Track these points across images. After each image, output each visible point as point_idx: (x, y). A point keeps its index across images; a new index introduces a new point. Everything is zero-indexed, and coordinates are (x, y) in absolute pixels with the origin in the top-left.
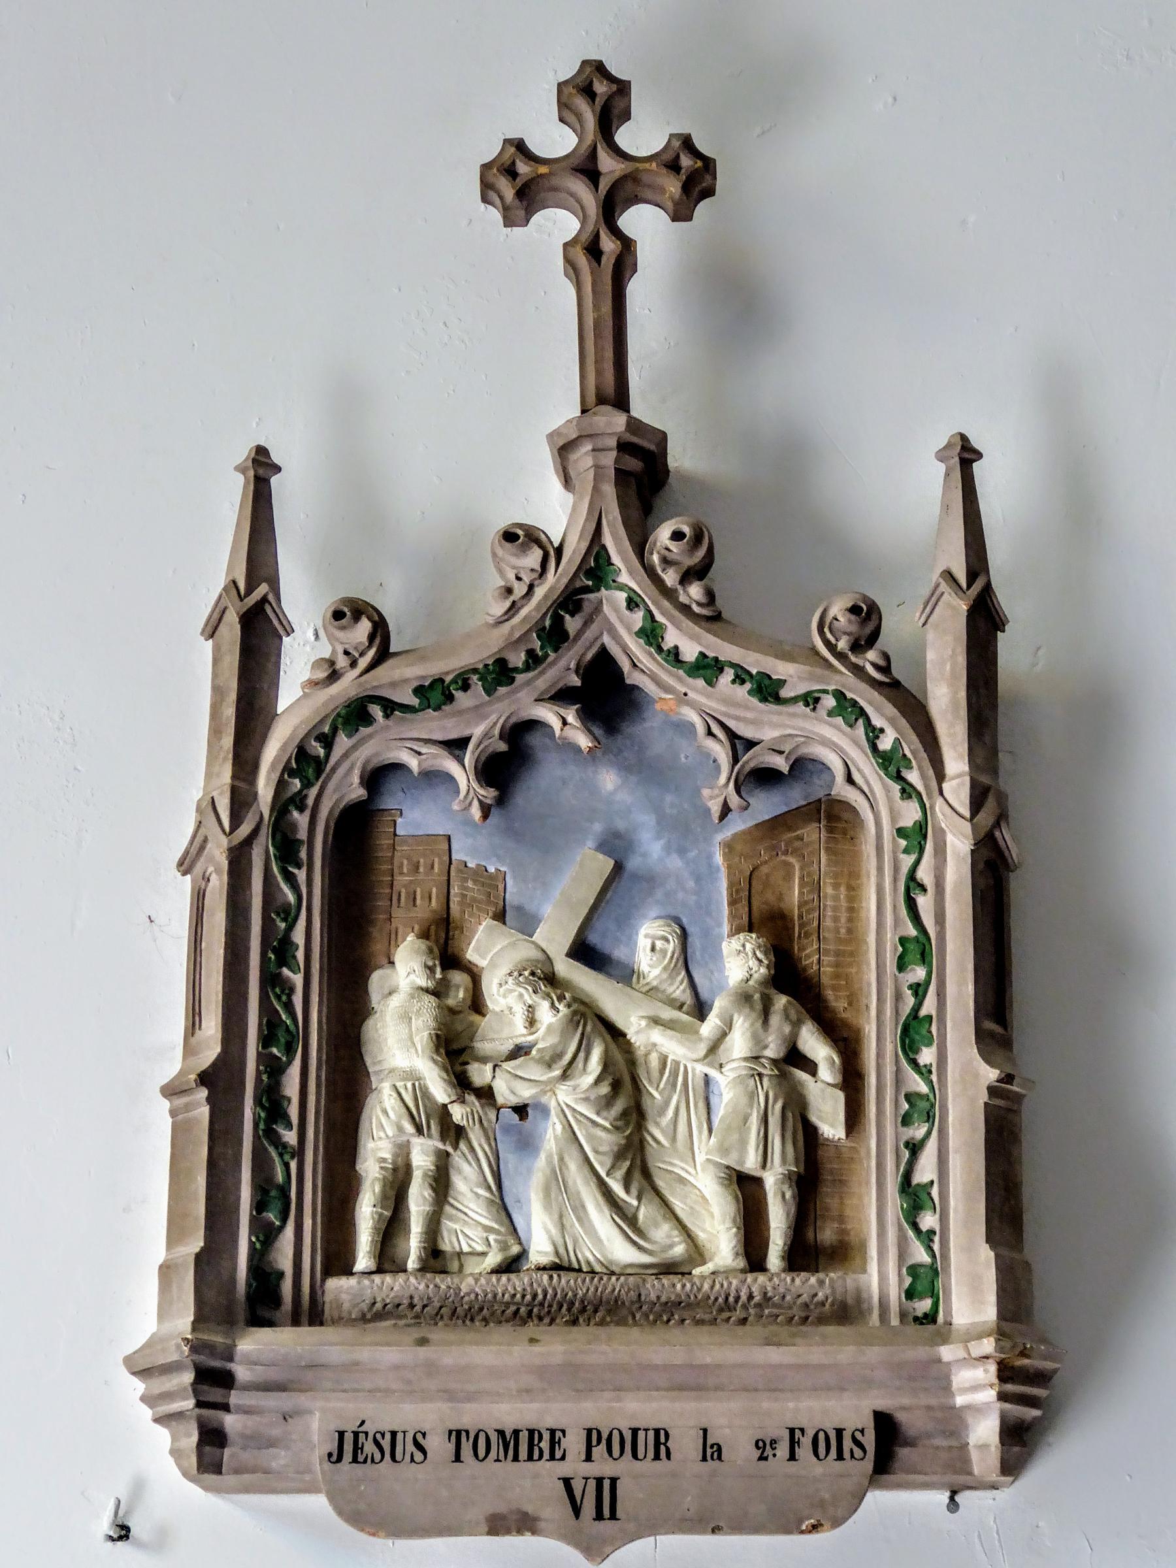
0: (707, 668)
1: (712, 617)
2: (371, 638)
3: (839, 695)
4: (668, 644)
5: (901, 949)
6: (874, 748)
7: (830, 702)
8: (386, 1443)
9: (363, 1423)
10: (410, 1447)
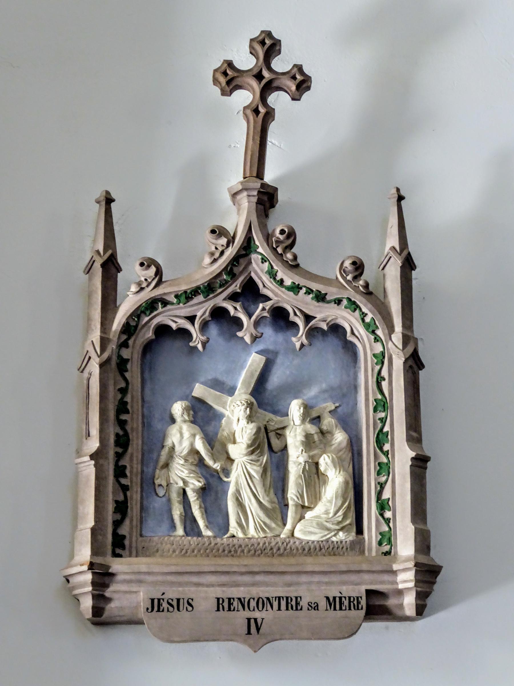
0: (295, 288)
1: (294, 266)
2: (156, 274)
3: (349, 300)
4: (278, 278)
5: (375, 403)
6: (363, 320)
7: (345, 302)
8: (175, 603)
9: (163, 594)
10: (186, 605)
